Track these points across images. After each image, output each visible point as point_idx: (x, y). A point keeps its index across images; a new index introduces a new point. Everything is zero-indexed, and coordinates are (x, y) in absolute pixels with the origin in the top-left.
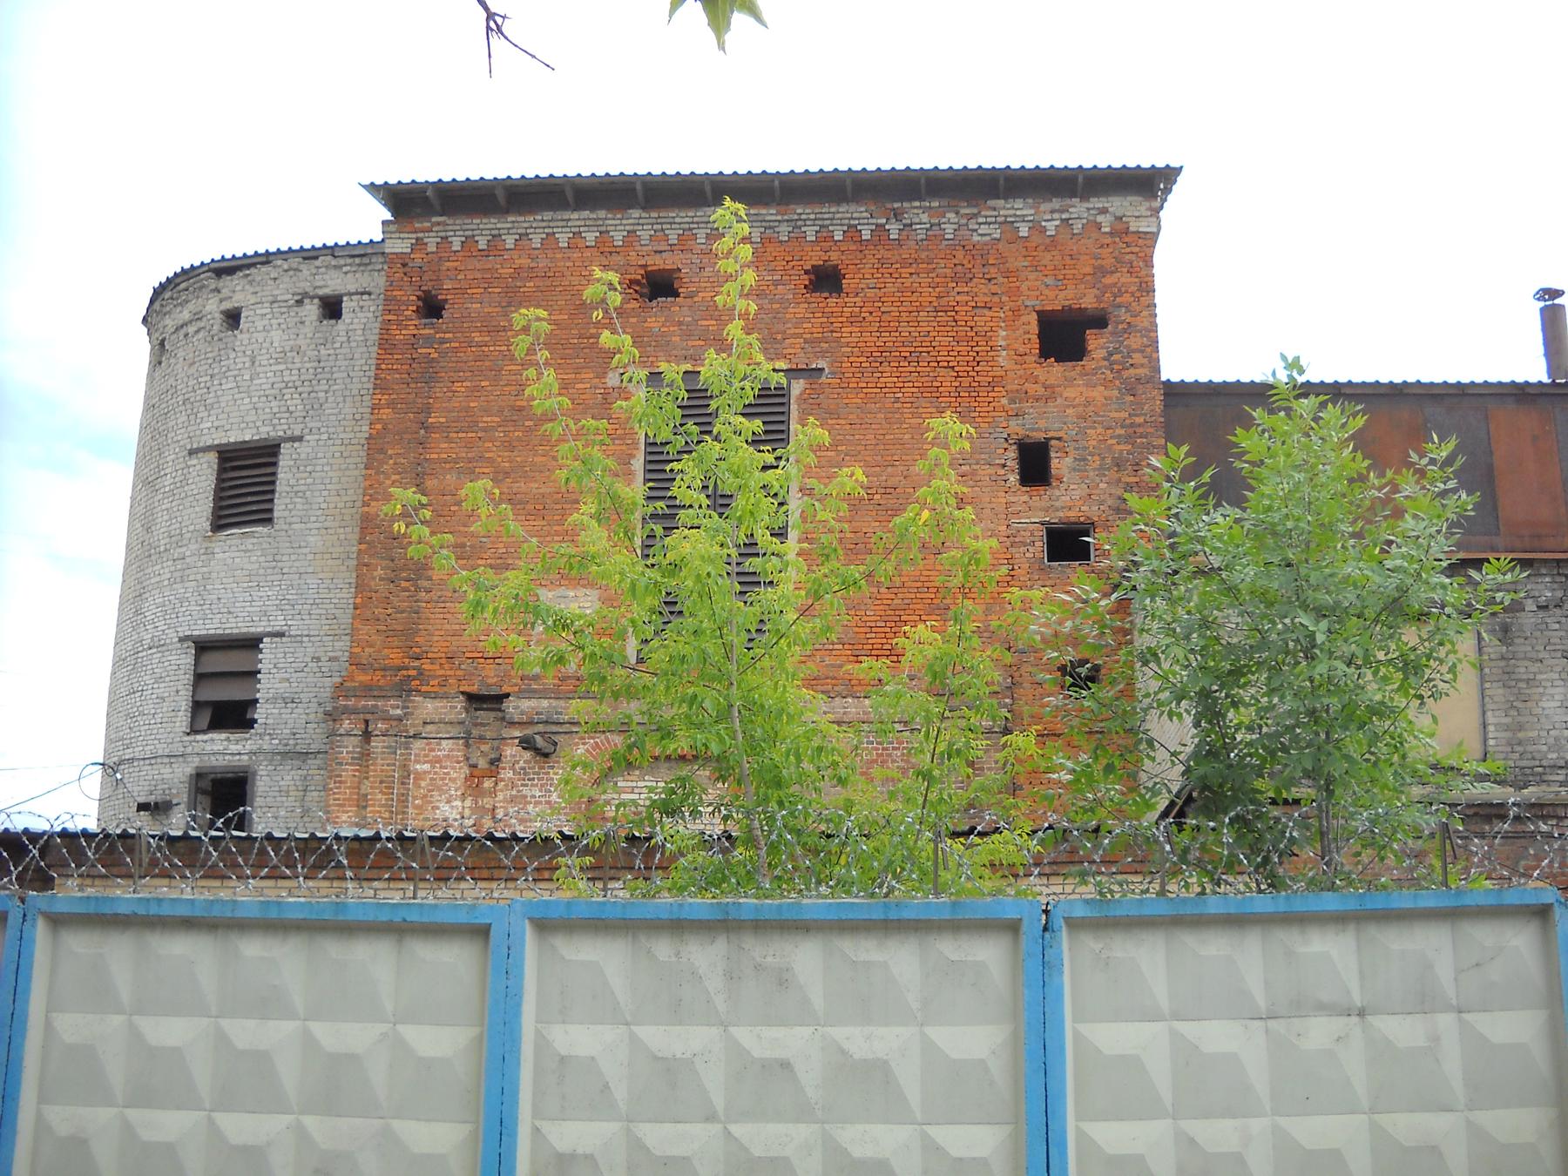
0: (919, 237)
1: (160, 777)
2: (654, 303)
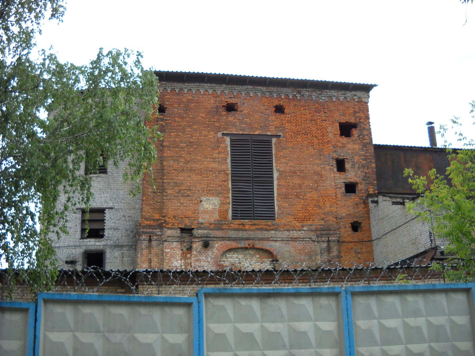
1: (71, 253)
2: (230, 113)
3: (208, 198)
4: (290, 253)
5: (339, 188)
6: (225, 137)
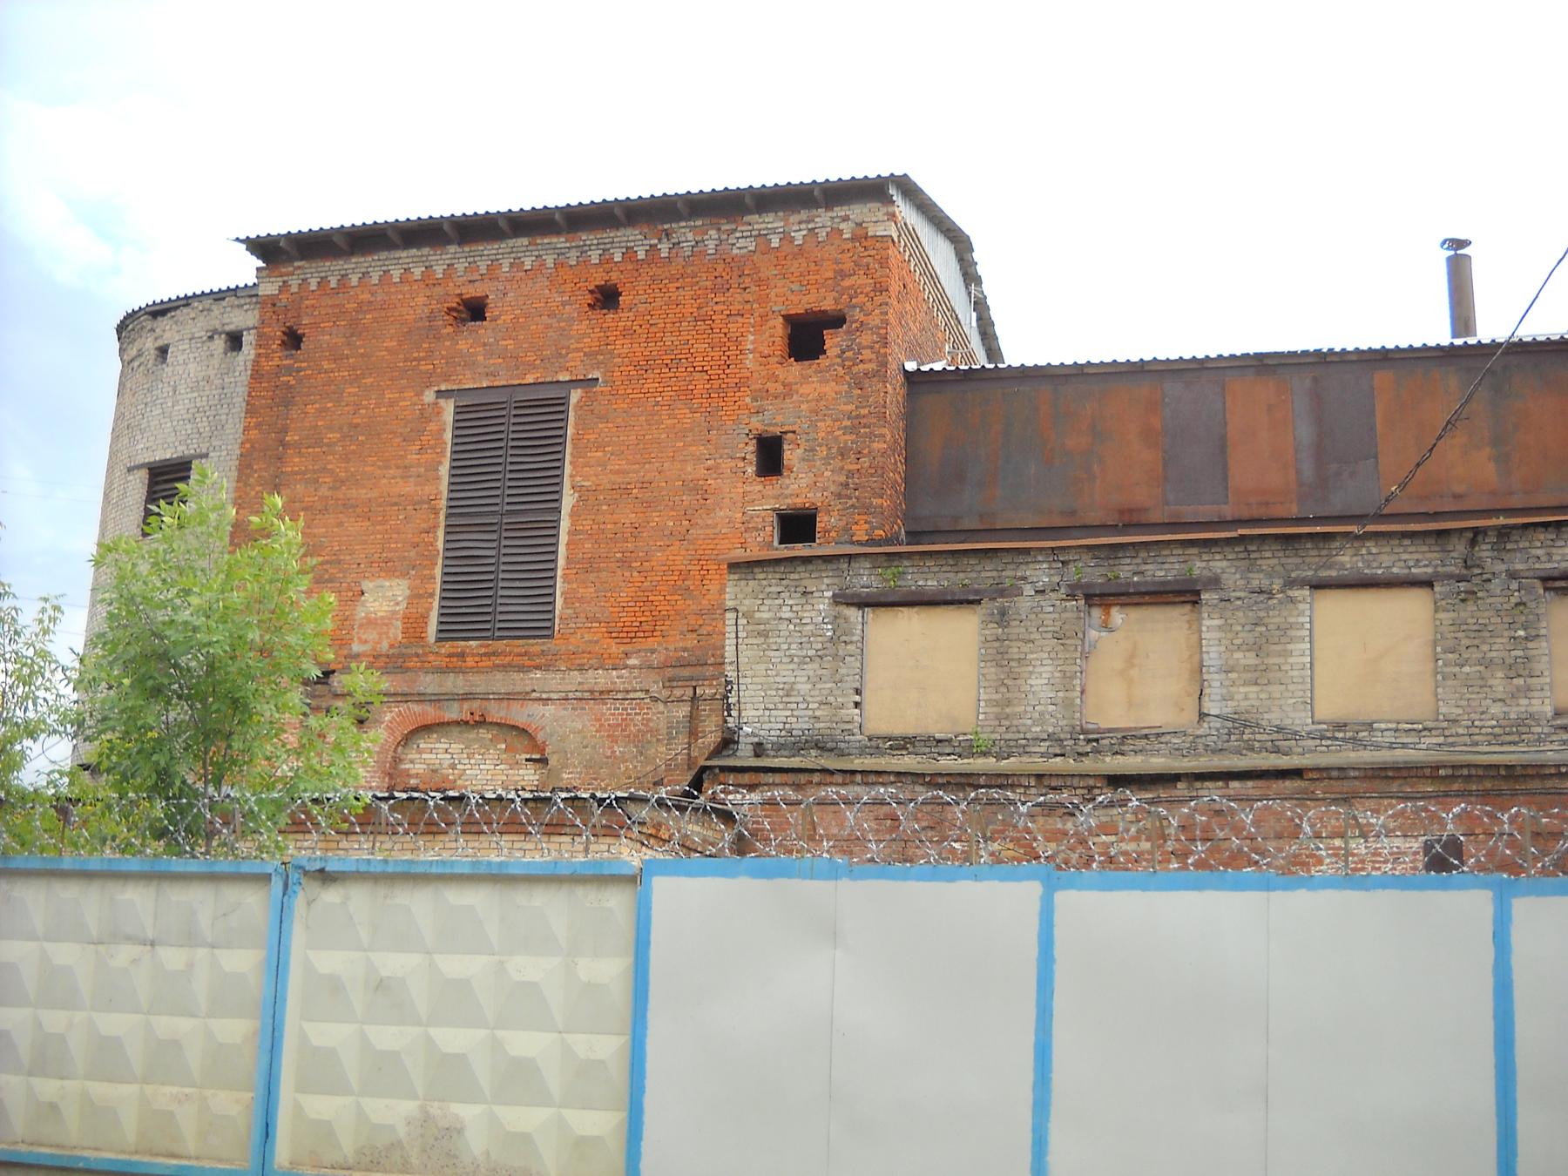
0: (687, 254)
3: (380, 582)
4: (584, 737)
5: (757, 529)
6: (442, 402)
